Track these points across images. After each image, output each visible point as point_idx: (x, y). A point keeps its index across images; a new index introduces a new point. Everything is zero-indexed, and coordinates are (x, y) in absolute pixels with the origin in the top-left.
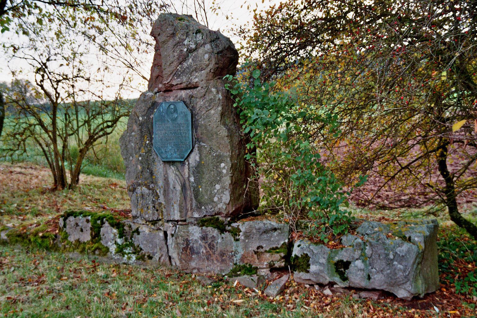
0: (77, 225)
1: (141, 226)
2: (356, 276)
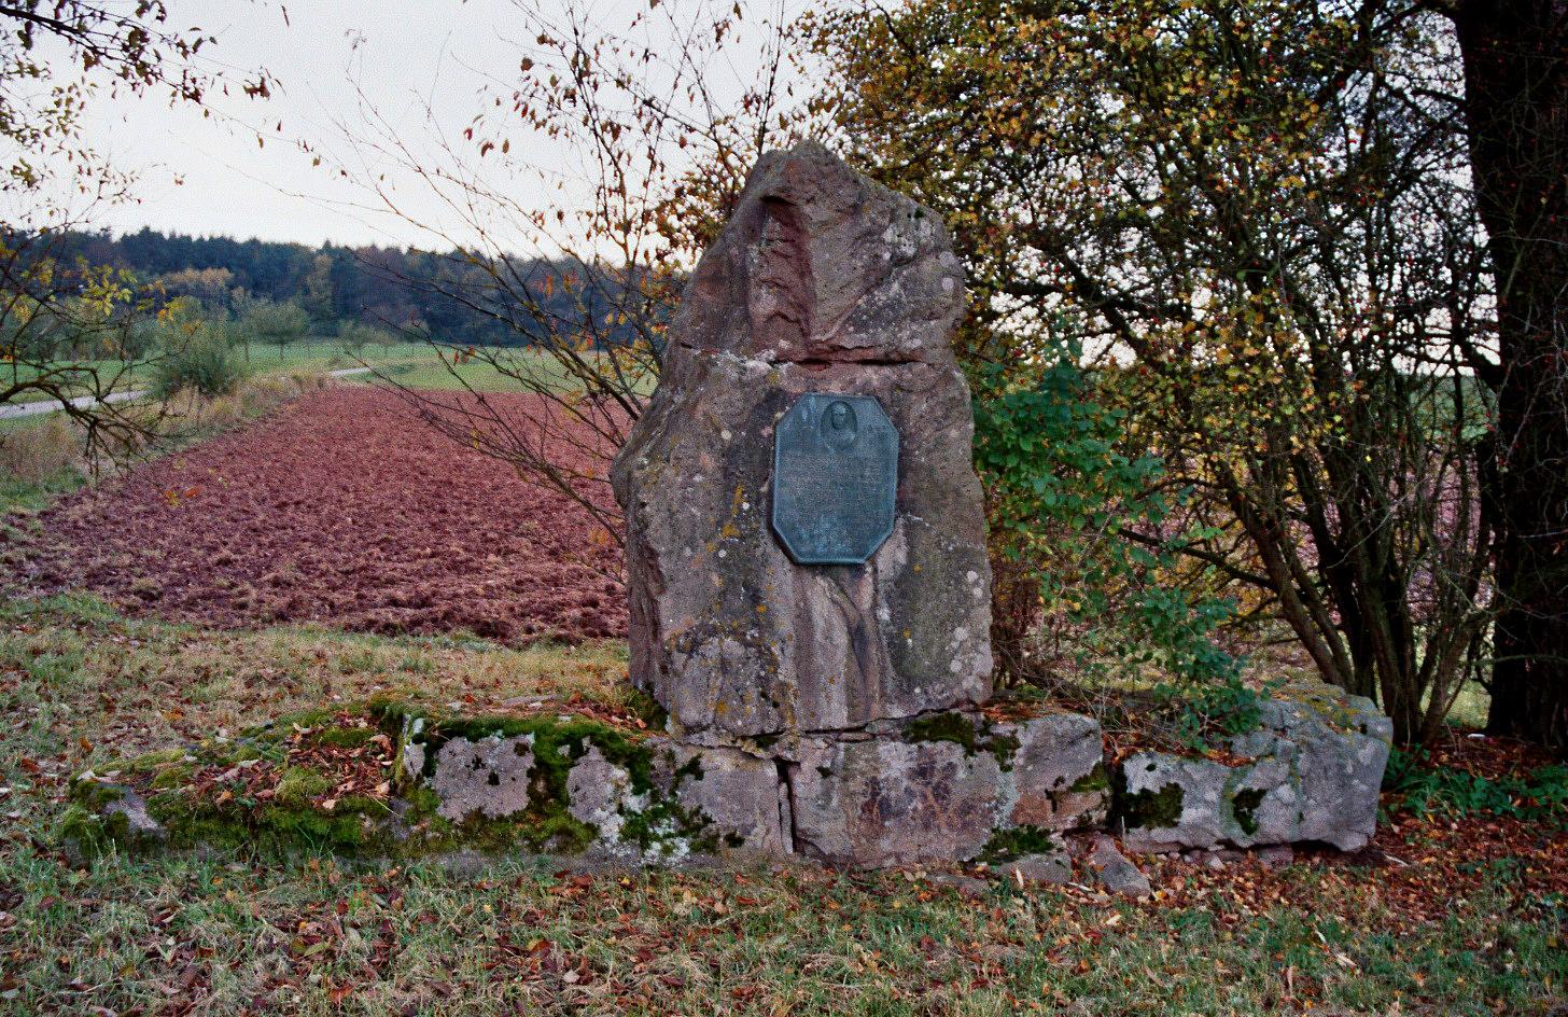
0: (478, 763)
1: (707, 752)
2: (1274, 821)
